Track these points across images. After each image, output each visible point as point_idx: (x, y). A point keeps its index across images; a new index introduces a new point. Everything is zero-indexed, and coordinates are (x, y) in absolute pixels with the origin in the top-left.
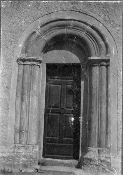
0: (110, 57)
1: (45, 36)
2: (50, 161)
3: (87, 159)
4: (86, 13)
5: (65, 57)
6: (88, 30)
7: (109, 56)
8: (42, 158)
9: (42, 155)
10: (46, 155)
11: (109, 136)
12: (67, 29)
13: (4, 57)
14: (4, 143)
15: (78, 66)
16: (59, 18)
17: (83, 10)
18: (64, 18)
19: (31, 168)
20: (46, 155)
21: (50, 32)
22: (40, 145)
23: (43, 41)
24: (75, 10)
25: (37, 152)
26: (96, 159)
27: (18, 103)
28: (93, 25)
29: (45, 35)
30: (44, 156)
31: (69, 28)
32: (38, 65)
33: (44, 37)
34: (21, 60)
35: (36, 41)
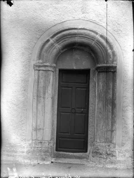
0: (117, 64)
1: (58, 44)
2: (62, 154)
3: (29, 141)
4: (96, 23)
5: (78, 62)
6: (98, 39)
7: (116, 63)
8: (55, 151)
9: (55, 149)
10: (59, 149)
11: (115, 133)
12: (79, 38)
13: (51, 45)
14: (22, 139)
15: (86, 73)
16: (70, 27)
17: (94, 19)
18: (75, 27)
19: (47, 161)
20: (59, 149)
21: (63, 40)
22: (54, 141)
23: (56, 49)
24: (85, 19)
25: (51, 147)
26: (103, 153)
27: (35, 105)
28: (102, 34)
29: (58, 43)
30: (56, 151)
31: (80, 37)
32: (52, 71)
33: (57, 45)
34: (37, 66)
35: (51, 47)
